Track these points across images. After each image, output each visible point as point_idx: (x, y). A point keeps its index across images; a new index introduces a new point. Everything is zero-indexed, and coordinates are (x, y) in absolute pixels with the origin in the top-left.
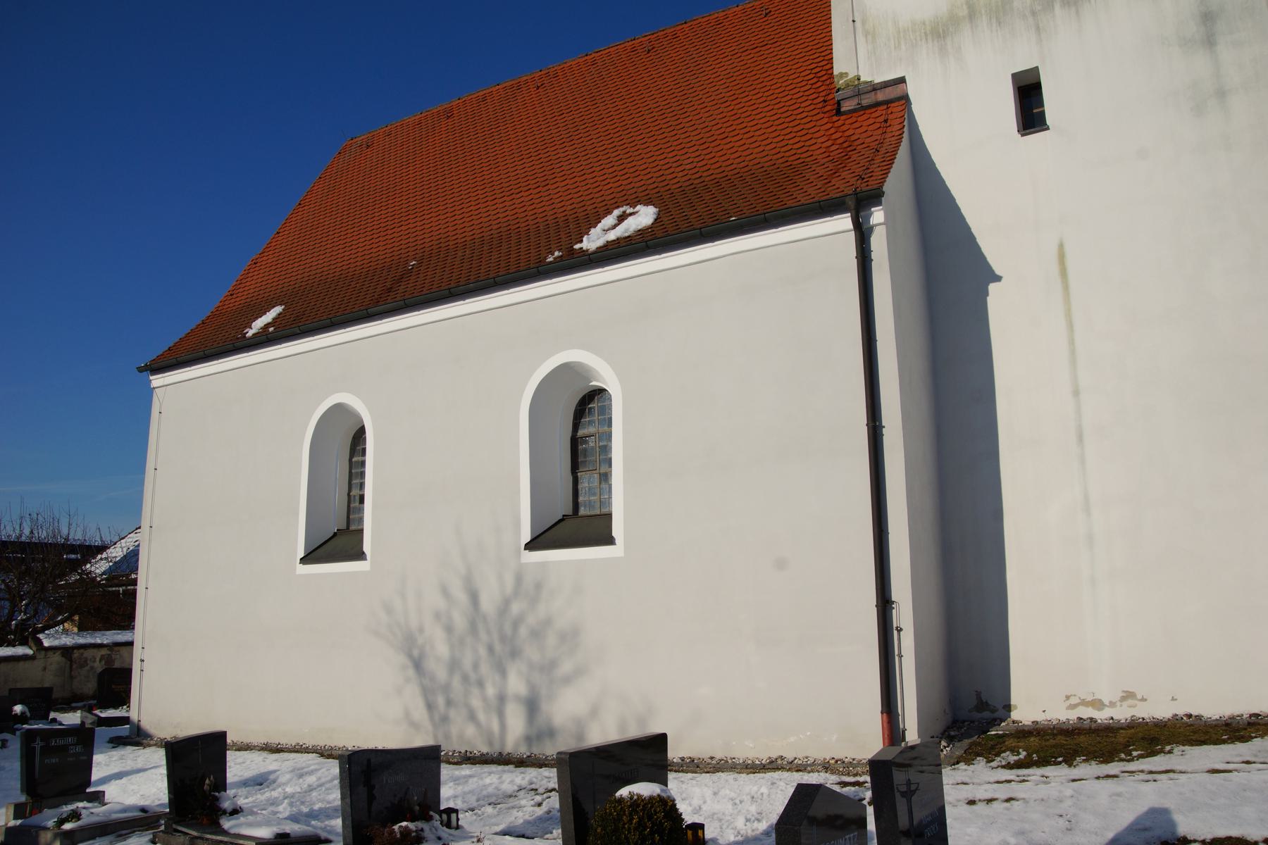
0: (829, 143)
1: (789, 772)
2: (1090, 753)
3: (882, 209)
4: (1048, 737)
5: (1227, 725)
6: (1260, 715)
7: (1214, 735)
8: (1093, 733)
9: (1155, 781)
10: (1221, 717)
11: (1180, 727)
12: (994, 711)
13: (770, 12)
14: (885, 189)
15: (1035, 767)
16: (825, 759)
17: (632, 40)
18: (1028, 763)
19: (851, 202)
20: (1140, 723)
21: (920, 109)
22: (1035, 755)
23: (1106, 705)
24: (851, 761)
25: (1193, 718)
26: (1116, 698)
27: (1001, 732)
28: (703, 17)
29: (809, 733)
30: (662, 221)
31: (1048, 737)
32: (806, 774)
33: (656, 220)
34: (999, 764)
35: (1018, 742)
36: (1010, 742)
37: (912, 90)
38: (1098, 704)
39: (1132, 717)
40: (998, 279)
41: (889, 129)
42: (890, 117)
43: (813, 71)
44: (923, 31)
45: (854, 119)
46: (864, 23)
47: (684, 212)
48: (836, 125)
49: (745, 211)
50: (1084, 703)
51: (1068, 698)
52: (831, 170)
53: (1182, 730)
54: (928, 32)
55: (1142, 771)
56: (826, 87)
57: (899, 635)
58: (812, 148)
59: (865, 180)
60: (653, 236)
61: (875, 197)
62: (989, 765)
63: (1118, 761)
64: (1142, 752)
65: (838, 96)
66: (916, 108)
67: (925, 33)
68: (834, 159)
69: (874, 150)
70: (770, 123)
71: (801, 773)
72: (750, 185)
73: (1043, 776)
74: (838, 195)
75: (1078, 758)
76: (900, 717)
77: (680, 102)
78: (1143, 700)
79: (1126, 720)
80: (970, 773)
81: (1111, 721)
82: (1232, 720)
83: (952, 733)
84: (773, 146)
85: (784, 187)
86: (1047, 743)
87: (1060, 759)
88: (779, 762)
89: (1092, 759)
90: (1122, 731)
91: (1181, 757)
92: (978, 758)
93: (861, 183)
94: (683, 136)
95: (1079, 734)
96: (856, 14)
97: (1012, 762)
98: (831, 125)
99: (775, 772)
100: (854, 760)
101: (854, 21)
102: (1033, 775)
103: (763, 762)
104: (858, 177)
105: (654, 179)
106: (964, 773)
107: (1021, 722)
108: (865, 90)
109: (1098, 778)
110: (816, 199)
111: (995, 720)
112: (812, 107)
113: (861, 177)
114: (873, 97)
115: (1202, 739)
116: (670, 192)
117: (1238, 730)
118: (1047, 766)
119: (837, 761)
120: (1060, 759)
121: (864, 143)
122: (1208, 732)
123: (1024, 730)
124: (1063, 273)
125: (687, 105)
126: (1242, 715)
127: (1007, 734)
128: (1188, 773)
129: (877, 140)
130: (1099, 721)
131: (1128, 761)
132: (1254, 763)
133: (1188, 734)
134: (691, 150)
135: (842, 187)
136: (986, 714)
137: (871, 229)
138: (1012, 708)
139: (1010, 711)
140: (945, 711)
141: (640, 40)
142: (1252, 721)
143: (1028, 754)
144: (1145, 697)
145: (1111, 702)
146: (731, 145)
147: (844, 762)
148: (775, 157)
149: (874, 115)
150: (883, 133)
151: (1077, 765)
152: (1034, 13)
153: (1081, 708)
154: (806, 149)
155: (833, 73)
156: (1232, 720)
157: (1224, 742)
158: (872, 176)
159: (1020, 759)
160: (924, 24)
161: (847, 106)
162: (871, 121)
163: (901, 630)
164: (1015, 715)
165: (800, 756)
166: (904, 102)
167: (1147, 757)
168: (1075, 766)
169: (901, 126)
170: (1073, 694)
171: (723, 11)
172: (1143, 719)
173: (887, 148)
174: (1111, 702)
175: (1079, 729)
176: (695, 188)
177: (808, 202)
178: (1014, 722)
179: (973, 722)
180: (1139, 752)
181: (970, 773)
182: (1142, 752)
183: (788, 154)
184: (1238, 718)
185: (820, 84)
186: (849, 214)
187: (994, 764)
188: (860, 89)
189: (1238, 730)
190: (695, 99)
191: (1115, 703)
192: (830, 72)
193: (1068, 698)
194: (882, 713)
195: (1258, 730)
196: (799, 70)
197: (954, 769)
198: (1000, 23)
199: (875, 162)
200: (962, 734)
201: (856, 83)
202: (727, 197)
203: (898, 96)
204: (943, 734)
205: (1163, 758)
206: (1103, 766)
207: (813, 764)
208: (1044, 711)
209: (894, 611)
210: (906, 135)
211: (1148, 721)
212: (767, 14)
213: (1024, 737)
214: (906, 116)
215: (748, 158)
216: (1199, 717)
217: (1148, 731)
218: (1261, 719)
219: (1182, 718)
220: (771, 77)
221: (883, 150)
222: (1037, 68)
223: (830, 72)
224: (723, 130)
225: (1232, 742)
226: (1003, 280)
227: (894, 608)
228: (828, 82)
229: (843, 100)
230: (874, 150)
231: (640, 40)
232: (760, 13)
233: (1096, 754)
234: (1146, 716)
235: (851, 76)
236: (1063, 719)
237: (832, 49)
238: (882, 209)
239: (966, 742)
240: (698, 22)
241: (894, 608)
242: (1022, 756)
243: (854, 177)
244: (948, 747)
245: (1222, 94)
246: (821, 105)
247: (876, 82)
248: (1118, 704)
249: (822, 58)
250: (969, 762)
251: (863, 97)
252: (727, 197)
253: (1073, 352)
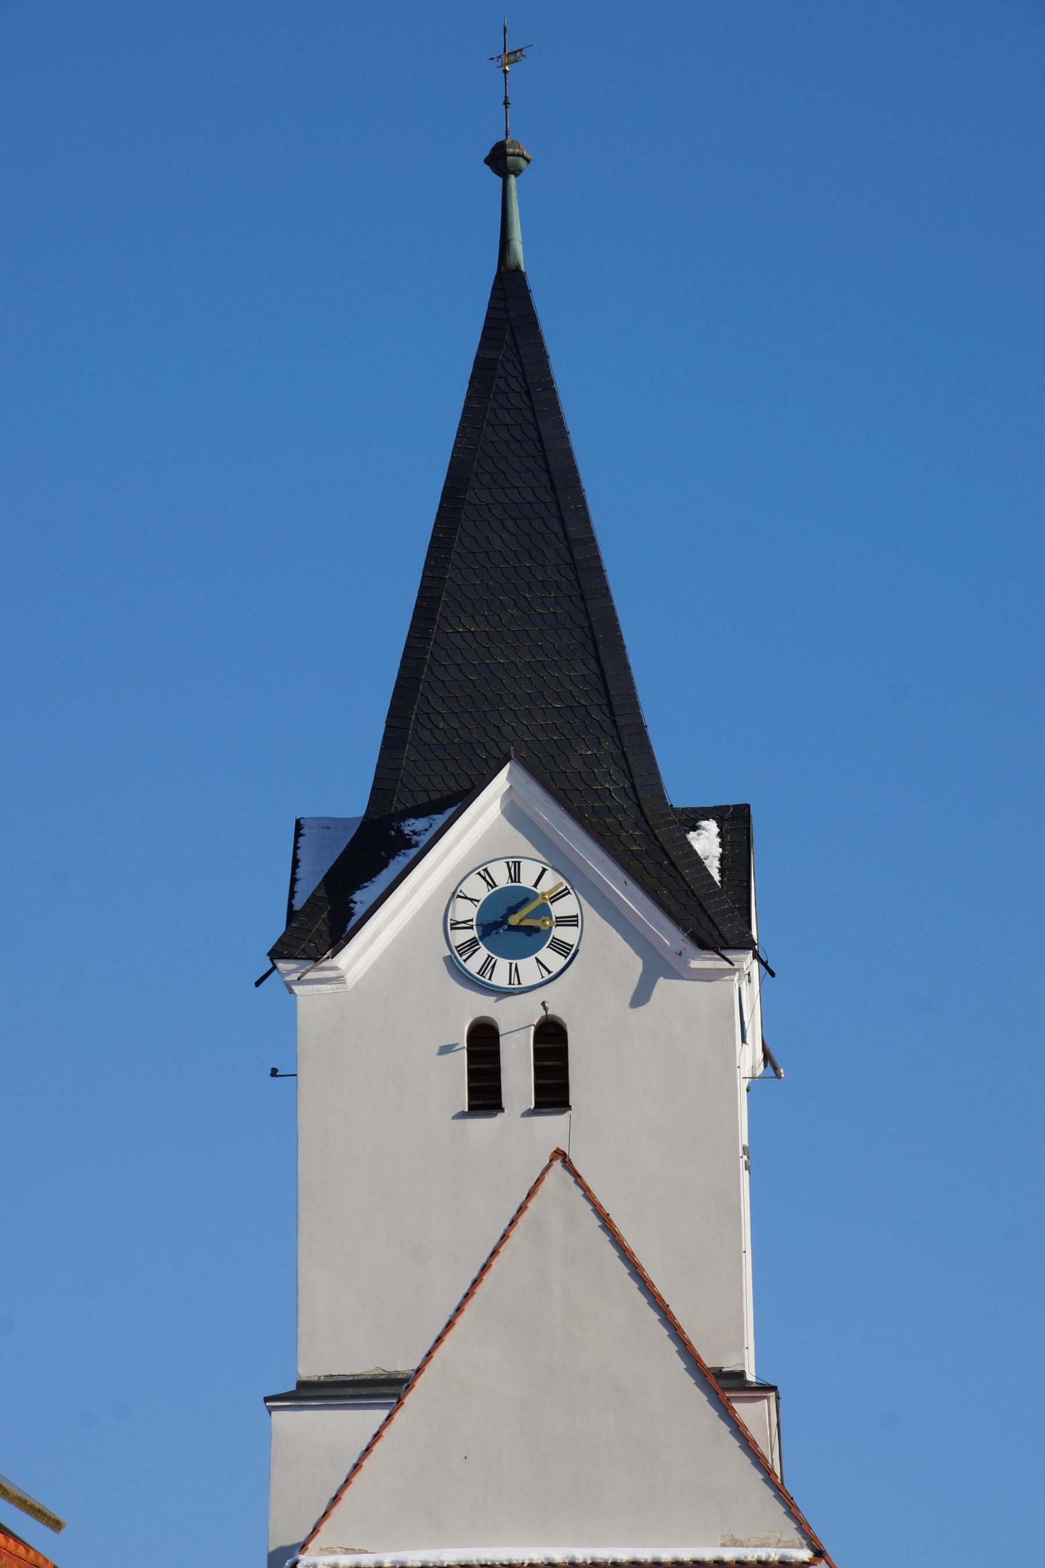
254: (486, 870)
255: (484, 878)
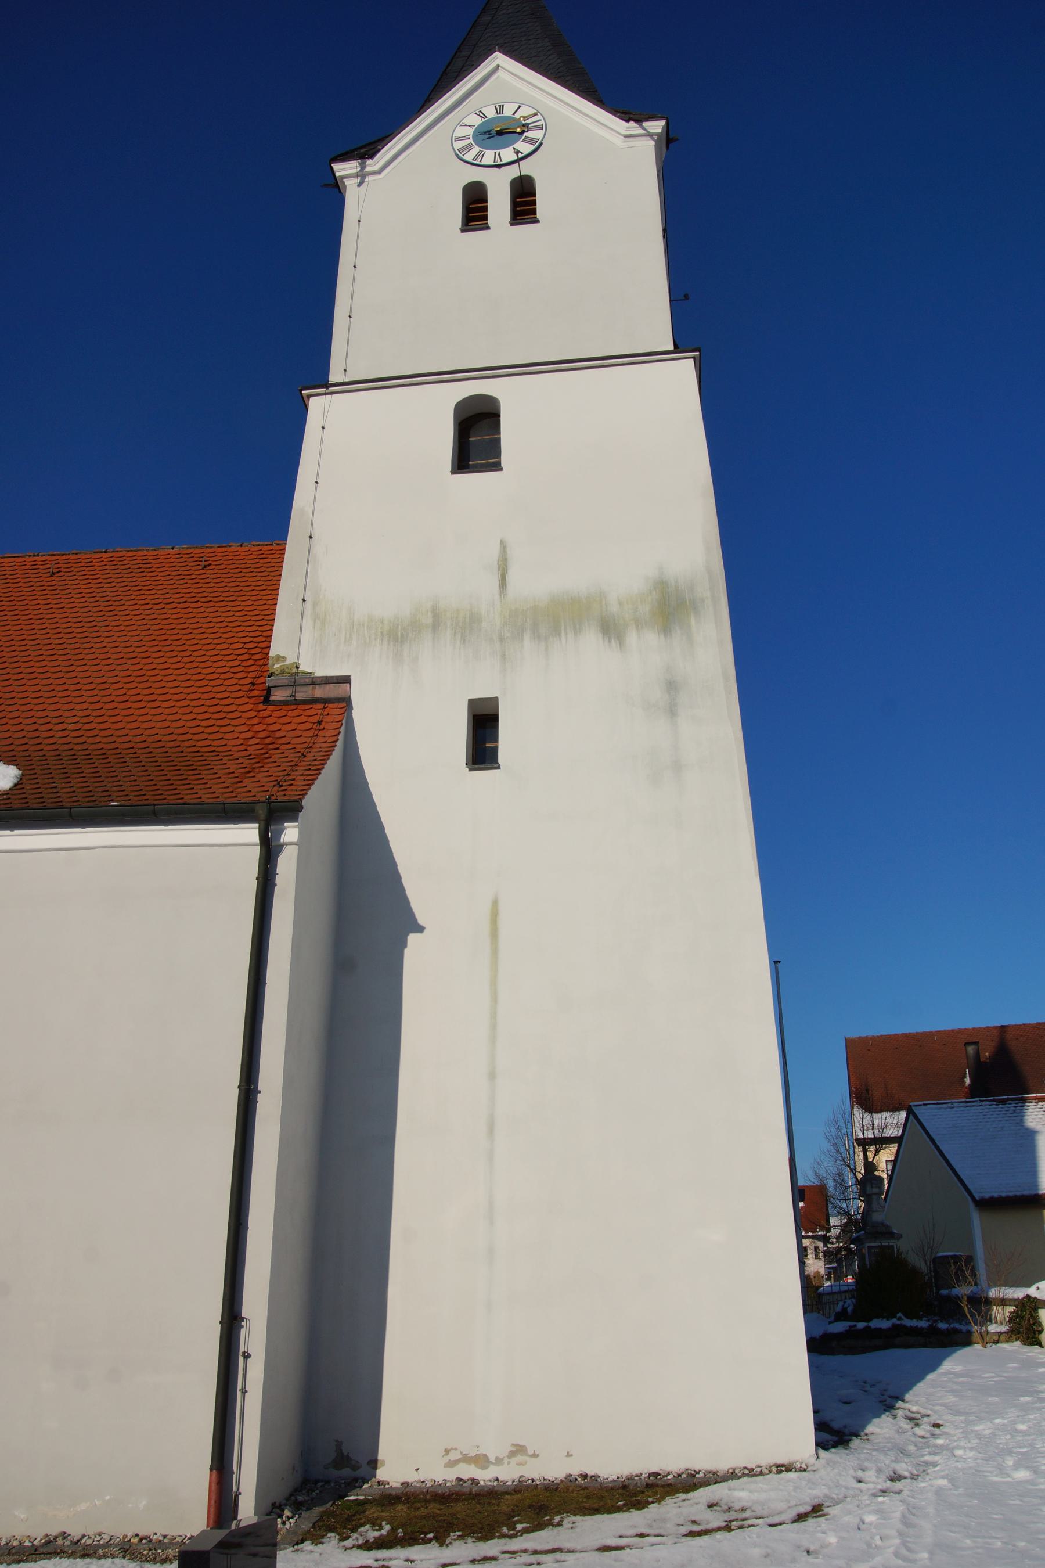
0: (249, 734)
1: (71, 1560)
2: (466, 1526)
3: (297, 826)
4: (419, 1505)
5: (624, 1487)
6: (660, 1475)
7: (609, 1501)
8: (473, 1499)
9: (539, 1564)
10: (618, 1478)
11: (573, 1492)
12: (355, 1467)
13: (210, 565)
14: (304, 802)
15: (399, 1547)
16: (125, 1536)
17: (34, 556)
18: (391, 1541)
19: (262, 811)
20: (528, 1486)
21: (361, 716)
22: (400, 1530)
23: (491, 1463)
24: (161, 1538)
25: (589, 1478)
26: (503, 1453)
27: (361, 1498)
28: (128, 551)
29: (108, 1498)
30: (23, 788)
31: (419, 1505)
32: (95, 1561)
33: (16, 785)
34: (355, 1542)
35: (382, 1511)
36: (372, 1511)
37: (356, 693)
38: (482, 1460)
39: (520, 1477)
40: (420, 929)
41: (321, 733)
42: (327, 719)
43: (247, 646)
44: (380, 630)
45: (282, 713)
46: (315, 604)
47: (54, 783)
48: (261, 714)
49: (131, 797)
50: (466, 1459)
51: (447, 1452)
52: (246, 767)
53: (575, 1495)
54: (385, 632)
55: (525, 1551)
56: (258, 668)
57: (245, 1363)
58: (227, 736)
59: (283, 788)
60: (9, 806)
61: (292, 810)
62: (342, 1544)
63: (499, 1537)
64: (529, 1525)
65: (270, 682)
66: (358, 714)
67: (382, 633)
68: (251, 755)
69: (300, 754)
70: (183, 696)
71: (88, 1560)
72: (144, 766)
73: (407, 1560)
74: (247, 800)
75: (452, 1534)
76: (234, 1476)
77: (77, 645)
78: (535, 1455)
79: (513, 1482)
80: (316, 1556)
81: (495, 1483)
82: (630, 1482)
83: (300, 1498)
84: (181, 723)
85: (186, 777)
86: (417, 1513)
87: (431, 1535)
88: (60, 1542)
89: (469, 1535)
90: (507, 1496)
91: (571, 1531)
92: (330, 1535)
93: (278, 791)
94: (73, 687)
95: (457, 1500)
96: (308, 593)
97: (371, 1540)
98: (255, 713)
99: (49, 1559)
100: (165, 1537)
101: (304, 600)
102: (396, 1559)
103: (35, 1543)
104: (276, 783)
105: (24, 733)
106: (308, 1557)
107: (388, 1484)
108: (302, 682)
109: (473, 1561)
110: (221, 799)
111: (356, 1480)
112: (238, 687)
113: (279, 783)
114: (310, 692)
115: (596, 1506)
116: (41, 753)
117: (635, 1494)
118: (413, 1545)
119: (141, 1540)
120: (431, 1535)
121: (289, 743)
122: (603, 1497)
123: (390, 1495)
124: (494, 934)
125: (86, 652)
126: (641, 1474)
127: (369, 1500)
128: (576, 1551)
129: (305, 743)
130: (482, 1483)
131: (511, 1537)
132: (648, 1535)
133: (580, 1500)
134: (78, 707)
135: (254, 791)
136: (346, 1472)
137: (280, 847)
138: (379, 1465)
139: (375, 1468)
140: (294, 1468)
141: (44, 558)
142: (651, 1482)
143: (392, 1529)
144: (537, 1453)
145: (497, 1458)
146: (131, 711)
147: (151, 1541)
148: (181, 738)
149: (308, 713)
150: (314, 736)
151: (451, 1543)
152: (502, 639)
153: (462, 1465)
154: (219, 736)
155: (269, 653)
156: (630, 1482)
157: (619, 1510)
158: (292, 785)
159: (382, 1535)
160: (382, 623)
161: (277, 695)
162: (303, 719)
163: (249, 1356)
164: (381, 1474)
165: (90, 1532)
166: (344, 704)
167: (533, 1531)
168: (447, 1546)
169: (336, 732)
170: (454, 1447)
171: (155, 550)
172: (533, 1480)
173: (316, 754)
174: (497, 1458)
175: (457, 1493)
176: (74, 755)
177: (210, 801)
178: (379, 1483)
179: (328, 1482)
180: (524, 1525)
181: (316, 1556)
182: (529, 1525)
183: (196, 737)
184: (637, 1478)
185: (251, 662)
186: (258, 825)
187: (348, 1543)
188: (296, 678)
189: (635, 1494)
190: (97, 646)
191: (502, 1459)
192: (266, 651)
193: (447, 1452)
194: (211, 1470)
195: (655, 1493)
196: (229, 641)
197: (297, 1550)
198: (464, 642)
199: (298, 768)
200: (312, 1499)
201: (294, 671)
202: (112, 774)
203: (340, 696)
204: (288, 1499)
205: (551, 1532)
206: (481, 1544)
207: (108, 1544)
208: (417, 1470)
209: (243, 1331)
210: (340, 744)
211: (538, 1483)
212: (205, 566)
213: (391, 1504)
214: (344, 722)
215: (148, 732)
216: (595, 1478)
217: (537, 1496)
218: (661, 1478)
219: (576, 1479)
220: (195, 642)
221: (310, 757)
222: (496, 698)
223: (266, 651)
224: (123, 691)
225: (628, 1510)
226: (425, 931)
227: (243, 1327)
228: (261, 662)
229: (275, 687)
230: (300, 754)
231: (44, 558)
232: (198, 563)
233: (475, 1528)
234: (536, 1476)
235: (289, 662)
236: (439, 1479)
237: (273, 626)
238: (297, 826)
239: (317, 1510)
240: (122, 554)
241: (243, 1327)
242: (384, 1532)
243: (271, 781)
244: (292, 1518)
245: (677, 767)
246: (247, 688)
247: (316, 675)
248: (506, 1461)
249: (260, 633)
250: (317, 1540)
251: (298, 688)
252: (112, 774)
253: (494, 1027)
254: (481, 111)
255: (464, 137)
